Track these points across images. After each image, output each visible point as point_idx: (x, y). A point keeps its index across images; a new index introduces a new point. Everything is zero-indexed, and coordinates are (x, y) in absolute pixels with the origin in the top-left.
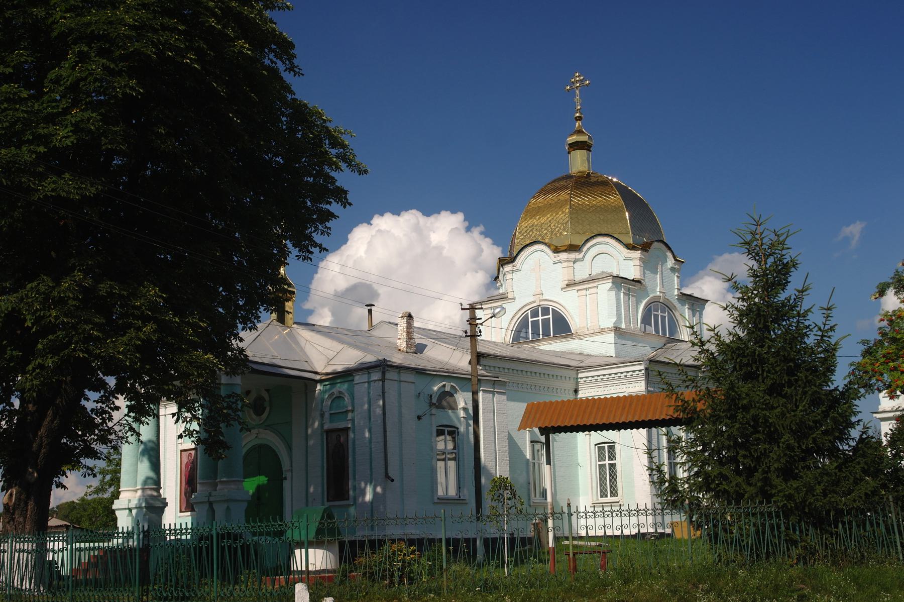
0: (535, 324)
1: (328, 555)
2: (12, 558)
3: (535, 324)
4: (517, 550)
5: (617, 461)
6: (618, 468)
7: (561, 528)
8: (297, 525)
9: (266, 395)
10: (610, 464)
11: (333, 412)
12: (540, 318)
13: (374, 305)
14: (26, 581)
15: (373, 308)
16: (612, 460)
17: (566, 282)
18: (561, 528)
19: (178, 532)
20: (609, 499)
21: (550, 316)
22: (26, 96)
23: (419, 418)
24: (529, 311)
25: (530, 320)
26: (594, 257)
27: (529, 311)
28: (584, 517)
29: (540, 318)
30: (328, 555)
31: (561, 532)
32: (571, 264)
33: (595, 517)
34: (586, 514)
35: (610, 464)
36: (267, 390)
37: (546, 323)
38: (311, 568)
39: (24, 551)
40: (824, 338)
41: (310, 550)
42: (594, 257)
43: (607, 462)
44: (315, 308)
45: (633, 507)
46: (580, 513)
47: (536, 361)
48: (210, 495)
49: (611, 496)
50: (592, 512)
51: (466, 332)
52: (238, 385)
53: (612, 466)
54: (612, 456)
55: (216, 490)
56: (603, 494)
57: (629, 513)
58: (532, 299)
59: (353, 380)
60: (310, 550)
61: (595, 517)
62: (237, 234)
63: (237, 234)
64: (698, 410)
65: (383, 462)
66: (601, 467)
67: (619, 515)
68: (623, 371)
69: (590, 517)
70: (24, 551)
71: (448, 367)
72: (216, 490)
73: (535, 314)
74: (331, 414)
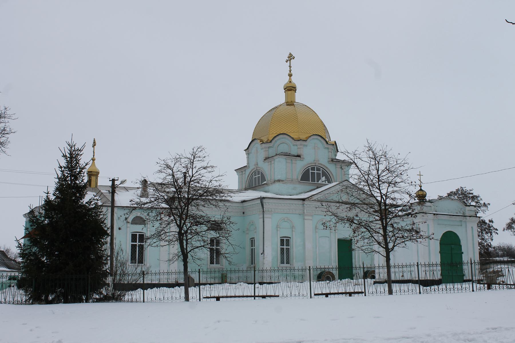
0: (313, 174)
5: (279, 247)
6: (291, 251)
16: (282, 246)
17: (264, 158)
20: (285, 265)
21: (260, 175)
24: (310, 167)
25: (310, 171)
26: (279, 145)
32: (267, 149)
33: (437, 266)
34: (429, 266)
38: (420, 279)
40: (183, 201)
41: (198, 282)
42: (279, 145)
43: (285, 247)
45: (396, 264)
47: (310, 191)
49: (286, 263)
53: (288, 250)
54: (288, 245)
56: (282, 262)
60: (198, 282)
61: (437, 266)
66: (282, 250)
68: (251, 204)
71: (243, 200)
73: (313, 169)
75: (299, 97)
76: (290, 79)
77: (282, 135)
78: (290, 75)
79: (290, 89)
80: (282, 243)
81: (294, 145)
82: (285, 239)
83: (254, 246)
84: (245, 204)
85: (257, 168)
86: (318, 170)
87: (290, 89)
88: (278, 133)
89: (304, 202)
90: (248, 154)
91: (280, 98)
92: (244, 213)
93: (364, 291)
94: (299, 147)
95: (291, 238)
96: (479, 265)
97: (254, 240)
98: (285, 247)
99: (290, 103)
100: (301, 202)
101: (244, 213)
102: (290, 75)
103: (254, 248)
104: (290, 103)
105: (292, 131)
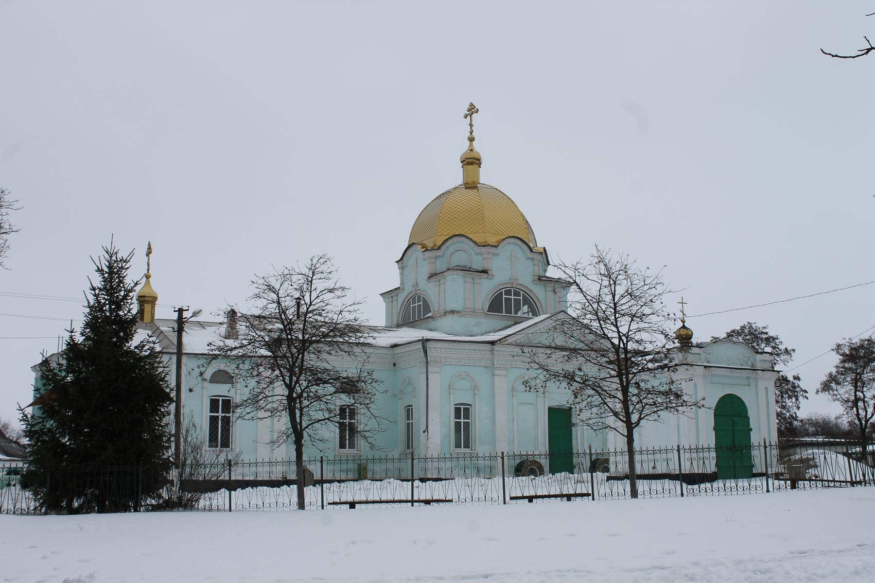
4: (176, 488)
5: (453, 420)
7: (673, 459)
10: (218, 412)
16: (458, 419)
18: (673, 459)
20: (463, 450)
21: (521, 298)
22: (526, 307)
24: (503, 290)
25: (504, 296)
31: (274, 475)
38: (683, 472)
41: (320, 479)
43: (462, 420)
45: (644, 449)
46: (699, 449)
49: (464, 447)
50: (358, 460)
53: (467, 425)
54: (467, 416)
56: (458, 445)
60: (320, 479)
62: (114, 340)
63: (114, 340)
64: (84, 338)
66: (458, 425)
69: (706, 451)
73: (508, 292)
75: (486, 176)
76: (471, 145)
78: (471, 140)
79: (471, 161)
83: (412, 419)
84: (397, 350)
85: (416, 291)
86: (517, 294)
87: (471, 161)
90: (402, 268)
91: (455, 177)
92: (395, 365)
95: (473, 406)
97: (412, 409)
98: (462, 420)
99: (471, 185)
101: (395, 365)
102: (471, 140)
103: (412, 423)
104: (471, 185)
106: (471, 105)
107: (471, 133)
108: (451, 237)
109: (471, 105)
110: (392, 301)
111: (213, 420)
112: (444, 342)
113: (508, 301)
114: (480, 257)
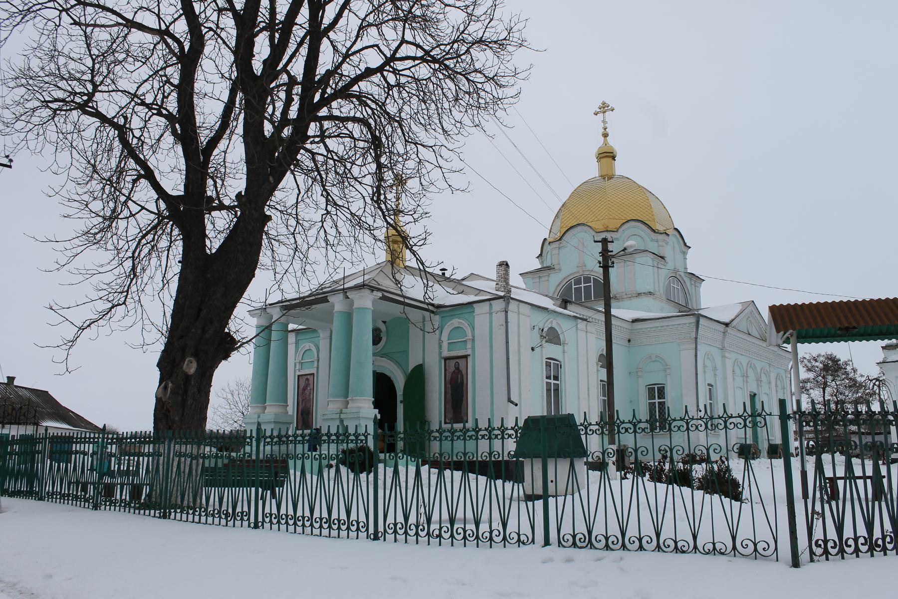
1: (678, 500)
2: (168, 465)
3: (578, 290)
8: (363, 438)
9: (382, 327)
10: (655, 399)
11: (450, 341)
12: (583, 285)
13: (446, 270)
14: (196, 471)
15: (445, 272)
19: (275, 440)
23: (533, 349)
24: (573, 280)
25: (573, 287)
27: (573, 280)
28: (499, 437)
29: (583, 285)
30: (678, 500)
35: (655, 399)
36: (384, 322)
37: (588, 289)
39: (185, 455)
43: (657, 401)
44: (560, 270)
48: (341, 413)
51: (600, 263)
52: (370, 309)
53: (662, 405)
55: (347, 408)
57: (635, 426)
58: (575, 270)
59: (474, 312)
65: (489, 391)
67: (499, 437)
69: (736, 425)
70: (185, 455)
72: (347, 408)
73: (578, 282)
74: (449, 343)
75: (621, 167)
76: (605, 141)
77: (626, 224)
78: (605, 135)
79: (607, 155)
80: (651, 395)
81: (652, 240)
82: (656, 386)
84: (639, 325)
85: (583, 271)
87: (607, 155)
88: (644, 220)
89: (727, 328)
91: (592, 170)
92: (629, 341)
93: (886, 475)
94: (660, 243)
95: (714, 386)
96: (745, 426)
98: (657, 401)
99: (607, 176)
100: (721, 328)
101: (629, 341)
102: (605, 135)
104: (607, 176)
105: (596, 219)
106: (604, 103)
107: (605, 129)
108: (627, 222)
109: (604, 103)
110: (539, 282)
111: (652, 406)
112: (707, 319)
113: (578, 290)
114: (656, 244)
